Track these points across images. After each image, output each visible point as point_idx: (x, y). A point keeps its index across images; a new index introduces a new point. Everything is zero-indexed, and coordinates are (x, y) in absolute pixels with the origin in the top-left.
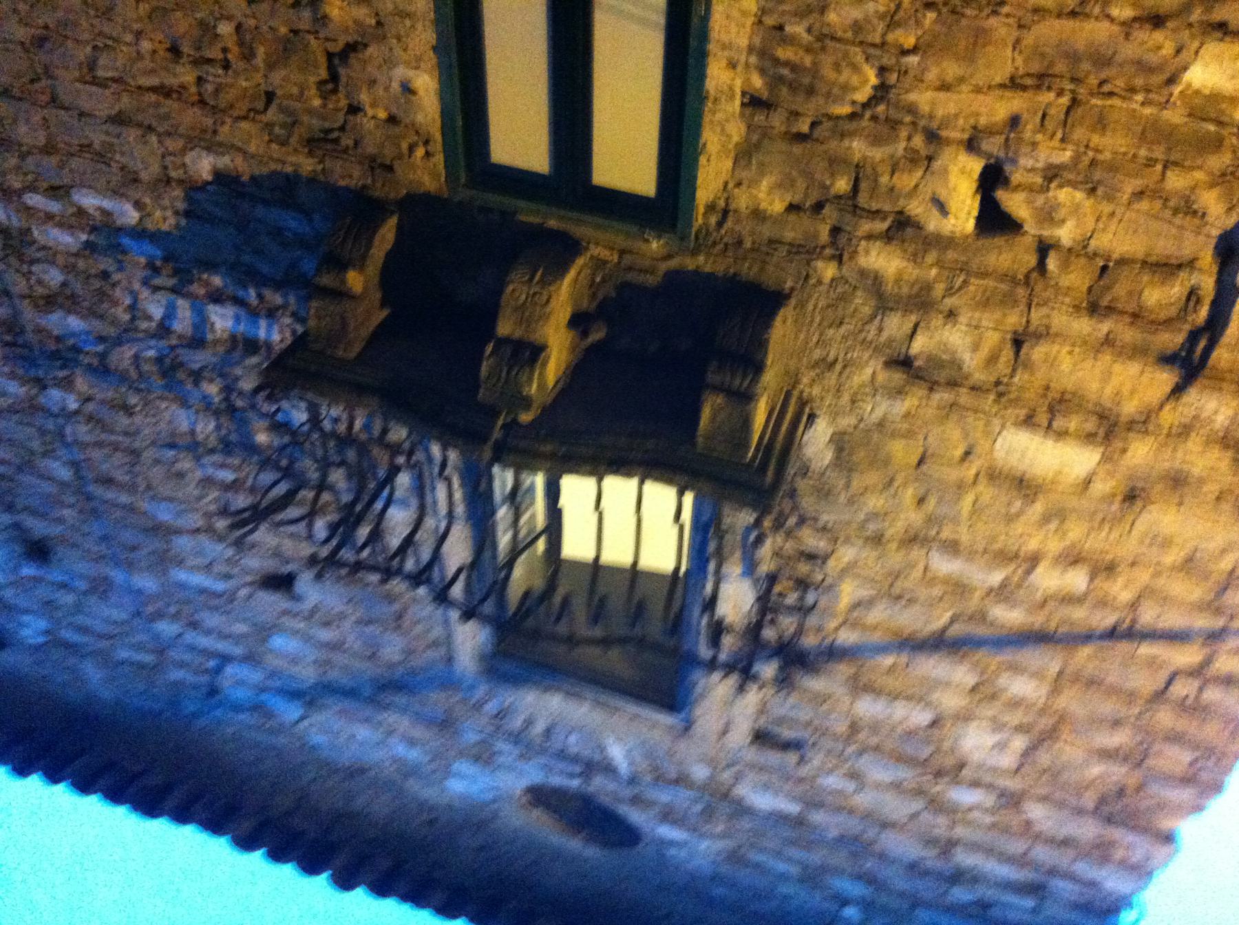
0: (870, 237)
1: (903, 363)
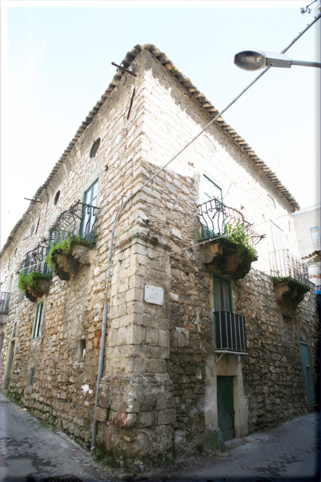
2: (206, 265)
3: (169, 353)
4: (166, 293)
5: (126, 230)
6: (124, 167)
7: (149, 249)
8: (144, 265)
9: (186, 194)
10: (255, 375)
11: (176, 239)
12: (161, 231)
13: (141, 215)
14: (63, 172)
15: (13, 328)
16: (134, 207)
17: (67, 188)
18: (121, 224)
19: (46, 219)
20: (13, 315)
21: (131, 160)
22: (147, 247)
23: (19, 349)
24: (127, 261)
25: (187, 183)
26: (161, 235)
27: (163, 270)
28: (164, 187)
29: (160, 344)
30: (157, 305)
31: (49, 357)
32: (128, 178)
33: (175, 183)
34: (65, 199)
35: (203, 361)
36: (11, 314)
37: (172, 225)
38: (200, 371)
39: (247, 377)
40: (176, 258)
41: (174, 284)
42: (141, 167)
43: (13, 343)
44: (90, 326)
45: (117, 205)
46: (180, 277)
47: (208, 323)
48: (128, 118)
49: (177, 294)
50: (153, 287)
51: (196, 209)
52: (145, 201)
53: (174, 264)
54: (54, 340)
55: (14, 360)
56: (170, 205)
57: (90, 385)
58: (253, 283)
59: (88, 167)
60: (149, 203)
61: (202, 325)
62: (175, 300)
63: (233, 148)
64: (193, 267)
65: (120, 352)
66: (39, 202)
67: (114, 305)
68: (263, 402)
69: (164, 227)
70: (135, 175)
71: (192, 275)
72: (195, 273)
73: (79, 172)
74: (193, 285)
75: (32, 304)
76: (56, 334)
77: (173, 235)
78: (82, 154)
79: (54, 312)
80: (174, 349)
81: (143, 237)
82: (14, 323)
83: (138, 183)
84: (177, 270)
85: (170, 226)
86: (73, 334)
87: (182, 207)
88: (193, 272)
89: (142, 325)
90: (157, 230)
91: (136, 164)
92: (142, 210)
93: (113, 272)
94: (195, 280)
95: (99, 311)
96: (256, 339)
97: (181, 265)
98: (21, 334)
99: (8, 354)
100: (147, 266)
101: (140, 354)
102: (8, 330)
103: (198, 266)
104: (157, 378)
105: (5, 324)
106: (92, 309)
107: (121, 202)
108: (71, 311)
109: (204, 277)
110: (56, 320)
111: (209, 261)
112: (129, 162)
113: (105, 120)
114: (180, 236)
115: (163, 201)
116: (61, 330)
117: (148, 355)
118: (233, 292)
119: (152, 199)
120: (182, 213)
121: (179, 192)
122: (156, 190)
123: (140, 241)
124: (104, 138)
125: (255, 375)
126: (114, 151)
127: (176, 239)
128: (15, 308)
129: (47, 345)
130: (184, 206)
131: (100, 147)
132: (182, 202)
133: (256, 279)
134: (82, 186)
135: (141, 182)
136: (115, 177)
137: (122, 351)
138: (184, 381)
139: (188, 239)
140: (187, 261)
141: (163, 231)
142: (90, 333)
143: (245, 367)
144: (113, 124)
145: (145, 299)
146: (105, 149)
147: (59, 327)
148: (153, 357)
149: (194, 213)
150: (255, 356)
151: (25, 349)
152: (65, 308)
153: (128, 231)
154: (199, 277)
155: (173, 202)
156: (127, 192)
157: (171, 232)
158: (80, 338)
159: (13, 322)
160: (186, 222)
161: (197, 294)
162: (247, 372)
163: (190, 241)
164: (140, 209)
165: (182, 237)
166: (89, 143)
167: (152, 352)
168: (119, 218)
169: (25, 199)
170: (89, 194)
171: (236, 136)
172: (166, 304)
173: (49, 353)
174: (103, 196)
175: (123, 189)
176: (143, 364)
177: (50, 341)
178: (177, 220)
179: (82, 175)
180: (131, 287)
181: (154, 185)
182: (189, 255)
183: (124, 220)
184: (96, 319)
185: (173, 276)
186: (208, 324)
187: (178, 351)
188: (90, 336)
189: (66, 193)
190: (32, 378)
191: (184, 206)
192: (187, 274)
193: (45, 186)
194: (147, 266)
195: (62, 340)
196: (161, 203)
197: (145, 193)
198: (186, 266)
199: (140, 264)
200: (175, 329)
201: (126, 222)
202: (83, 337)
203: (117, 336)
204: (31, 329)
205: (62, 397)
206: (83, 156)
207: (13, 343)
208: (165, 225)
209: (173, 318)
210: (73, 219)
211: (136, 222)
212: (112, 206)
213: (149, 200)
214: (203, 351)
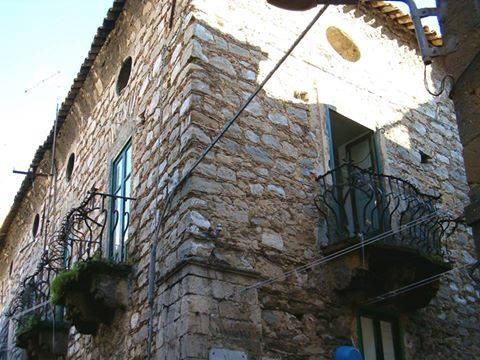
0: (322, 311)
2: (339, 292)
5: (173, 246)
6: (166, 122)
7: (215, 283)
8: (204, 314)
9: (292, 159)
11: (273, 253)
12: (238, 244)
13: (195, 221)
14: (76, 118)
17: (85, 150)
18: (167, 235)
19: (55, 209)
21: (177, 111)
22: (210, 279)
24: (176, 306)
25: (293, 137)
26: (238, 251)
27: (245, 316)
33: (267, 142)
34: (83, 172)
37: (262, 227)
40: (274, 289)
45: (160, 197)
46: (283, 325)
48: (171, 27)
50: (225, 351)
53: (269, 303)
58: (456, 311)
59: (115, 112)
66: (41, 175)
69: (245, 234)
71: (309, 317)
72: (316, 312)
73: (103, 120)
74: (314, 336)
78: (105, 87)
81: (202, 262)
85: (258, 229)
88: (310, 311)
91: (184, 120)
93: (157, 325)
94: (317, 325)
97: (284, 302)
103: (321, 296)
107: (165, 191)
109: (337, 317)
112: (175, 113)
113: (137, 24)
114: (280, 246)
115: (241, 184)
118: (405, 337)
119: (219, 186)
121: (275, 158)
122: (225, 165)
123: (195, 270)
124: (138, 58)
126: (154, 87)
127: (273, 253)
130: (288, 185)
131: (132, 75)
132: (282, 177)
133: (463, 301)
134: (109, 150)
136: (155, 140)
139: (298, 248)
140: (298, 292)
141: (242, 243)
144: (149, 31)
146: (139, 80)
153: (176, 249)
157: (260, 242)
160: (292, 215)
161: (323, 352)
163: (303, 251)
164: (191, 209)
166: (114, 65)
168: (164, 220)
169: (15, 172)
170: (120, 165)
171: (398, 15)
174: (138, 175)
175: (168, 166)
179: (107, 128)
181: (221, 156)
182: (301, 279)
183: (170, 229)
185: (268, 325)
189: (84, 160)
191: (288, 185)
192: (299, 316)
193: (49, 145)
198: (295, 301)
199: (197, 313)
201: (175, 231)
206: (106, 91)
208: (247, 230)
210: (85, 227)
212: (153, 198)
213: (211, 187)
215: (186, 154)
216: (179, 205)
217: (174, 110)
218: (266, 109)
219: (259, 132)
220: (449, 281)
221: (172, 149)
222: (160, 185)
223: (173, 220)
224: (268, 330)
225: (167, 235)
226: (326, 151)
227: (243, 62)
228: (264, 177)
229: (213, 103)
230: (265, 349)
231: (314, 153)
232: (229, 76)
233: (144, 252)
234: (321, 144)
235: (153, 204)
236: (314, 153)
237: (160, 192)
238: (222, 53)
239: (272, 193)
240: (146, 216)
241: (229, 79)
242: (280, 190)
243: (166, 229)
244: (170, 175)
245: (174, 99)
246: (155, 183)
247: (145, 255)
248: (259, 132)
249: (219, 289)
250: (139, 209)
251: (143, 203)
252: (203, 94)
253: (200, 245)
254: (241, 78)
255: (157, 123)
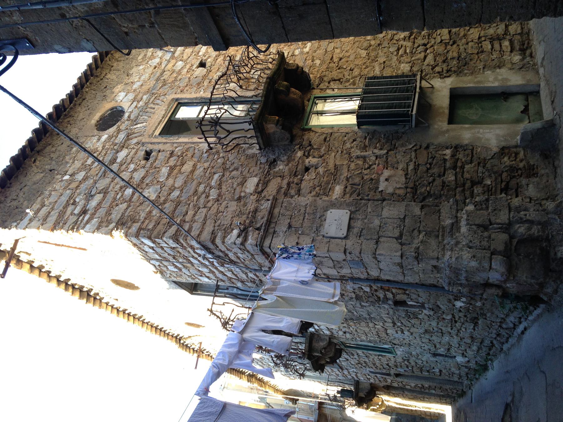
1: (275, 160)
3: (413, 203)
4: (333, 205)
5: (250, 257)
6: (160, 256)
8: (298, 238)
9: (195, 166)
10: (450, 55)
13: (232, 240)
15: (378, 375)
16: (220, 248)
18: (243, 260)
20: (359, 375)
21: (152, 248)
23: (407, 369)
26: (256, 211)
28: (188, 202)
29: (402, 217)
30: (350, 219)
31: (417, 338)
32: (178, 252)
33: (180, 184)
35: (427, 147)
36: (357, 377)
37: (241, 192)
38: (440, 152)
39: (453, 69)
40: (286, 187)
41: (322, 191)
42: (164, 239)
43: (397, 375)
44: (376, 296)
45: (216, 264)
47: (373, 137)
49: (334, 187)
51: (214, 150)
52: (212, 234)
53: (295, 191)
54: (395, 332)
55: (422, 375)
56: (214, 194)
57: (455, 300)
58: (315, 51)
60: (215, 226)
61: (376, 148)
62: (342, 191)
63: (108, 76)
64: (297, 159)
65: (411, 269)
67: (350, 271)
68: (492, 40)
69: (245, 205)
70: (174, 245)
75: (345, 353)
76: (386, 330)
77: (256, 191)
79: (356, 331)
80: (408, 195)
82: (370, 374)
83: (187, 243)
84: (302, 186)
86: (386, 312)
87: (215, 173)
89: (377, 243)
90: (250, 216)
91: (159, 244)
92: (225, 237)
95: (356, 286)
96: (398, 49)
98: (385, 366)
99: (415, 382)
100: (300, 232)
101: (414, 246)
102: (380, 381)
104: (446, 223)
105: (371, 384)
106: (354, 293)
107: (211, 260)
108: (355, 313)
110: (367, 330)
111: (288, 135)
112: (154, 250)
114: (255, 180)
115: (209, 205)
116: (381, 324)
117: (416, 235)
119: (208, 222)
120: (223, 176)
122: (194, 215)
123: (267, 243)
125: (450, 55)
127: (260, 185)
128: (349, 372)
129: (402, 339)
132: (207, 175)
135: (186, 240)
136: (174, 265)
137: (409, 267)
138: (453, 178)
139: (258, 166)
140: (289, 169)
141: (251, 207)
142: (385, 295)
143: (439, 72)
145: (343, 236)
147: (376, 326)
148: (419, 227)
149: (221, 155)
150: (423, 55)
151: (406, 362)
152: (352, 319)
153: (252, 255)
154: (310, 150)
155: (208, 188)
156: (197, 253)
157: (251, 194)
158: (393, 307)
159: (369, 375)
162: (445, 68)
164: (223, 242)
165: (256, 176)
167: (412, 229)
168: (232, 262)
169: (196, 368)
172: (348, 205)
173: (411, 338)
175: (193, 257)
176: (427, 242)
177: (396, 335)
178: (233, 184)
180: (327, 255)
181: (188, 218)
184: (368, 289)
186: (375, 137)
187: (412, 188)
188: (390, 295)
190: (446, 356)
192: (307, 169)
194: (300, 232)
195: (394, 324)
196: (212, 208)
197: (201, 232)
198: (296, 172)
200: (382, 191)
201: (239, 255)
202: (390, 302)
203: (390, 271)
204: (379, 355)
205: (472, 327)
207: (397, 375)
208: (242, 203)
209: (367, 194)
211: (242, 247)
212: (216, 268)
213: (209, 228)
214: (413, 147)
215: (185, 244)
216: (221, 251)
217: (151, 251)
218: (155, 182)
219: (172, 189)
220: (293, 55)
221: (180, 253)
222: (207, 263)
223: (231, 255)
224: (314, 193)
225: (243, 260)
226: (190, 140)
227: (118, 197)
228: (206, 187)
229: (147, 221)
230: (327, 196)
231: (191, 150)
232: (127, 209)
233: (255, 277)
234: (186, 143)
235: (221, 269)
236: (191, 150)
237: (212, 263)
238: (109, 213)
239: (218, 183)
240: (229, 274)
241: (131, 208)
242: (216, 177)
243: (238, 261)
244: (200, 256)
245: (143, 250)
246: (206, 266)
247: (257, 276)
248: (172, 189)
249: (282, 228)
250: (224, 278)
251: (220, 276)
252: (140, 229)
253: (250, 237)
254: (130, 200)
255: (161, 263)
